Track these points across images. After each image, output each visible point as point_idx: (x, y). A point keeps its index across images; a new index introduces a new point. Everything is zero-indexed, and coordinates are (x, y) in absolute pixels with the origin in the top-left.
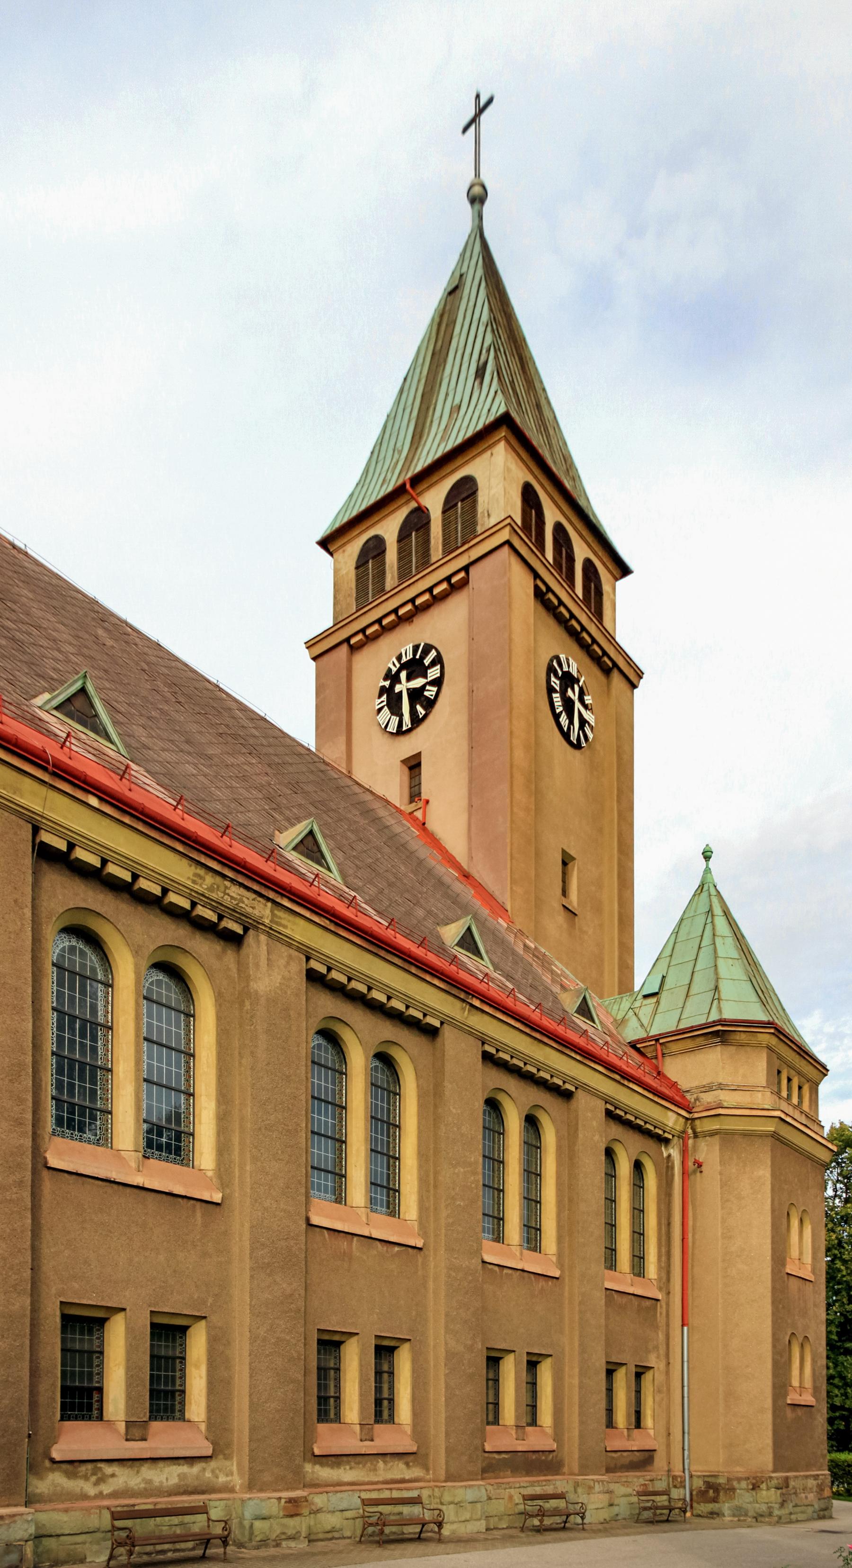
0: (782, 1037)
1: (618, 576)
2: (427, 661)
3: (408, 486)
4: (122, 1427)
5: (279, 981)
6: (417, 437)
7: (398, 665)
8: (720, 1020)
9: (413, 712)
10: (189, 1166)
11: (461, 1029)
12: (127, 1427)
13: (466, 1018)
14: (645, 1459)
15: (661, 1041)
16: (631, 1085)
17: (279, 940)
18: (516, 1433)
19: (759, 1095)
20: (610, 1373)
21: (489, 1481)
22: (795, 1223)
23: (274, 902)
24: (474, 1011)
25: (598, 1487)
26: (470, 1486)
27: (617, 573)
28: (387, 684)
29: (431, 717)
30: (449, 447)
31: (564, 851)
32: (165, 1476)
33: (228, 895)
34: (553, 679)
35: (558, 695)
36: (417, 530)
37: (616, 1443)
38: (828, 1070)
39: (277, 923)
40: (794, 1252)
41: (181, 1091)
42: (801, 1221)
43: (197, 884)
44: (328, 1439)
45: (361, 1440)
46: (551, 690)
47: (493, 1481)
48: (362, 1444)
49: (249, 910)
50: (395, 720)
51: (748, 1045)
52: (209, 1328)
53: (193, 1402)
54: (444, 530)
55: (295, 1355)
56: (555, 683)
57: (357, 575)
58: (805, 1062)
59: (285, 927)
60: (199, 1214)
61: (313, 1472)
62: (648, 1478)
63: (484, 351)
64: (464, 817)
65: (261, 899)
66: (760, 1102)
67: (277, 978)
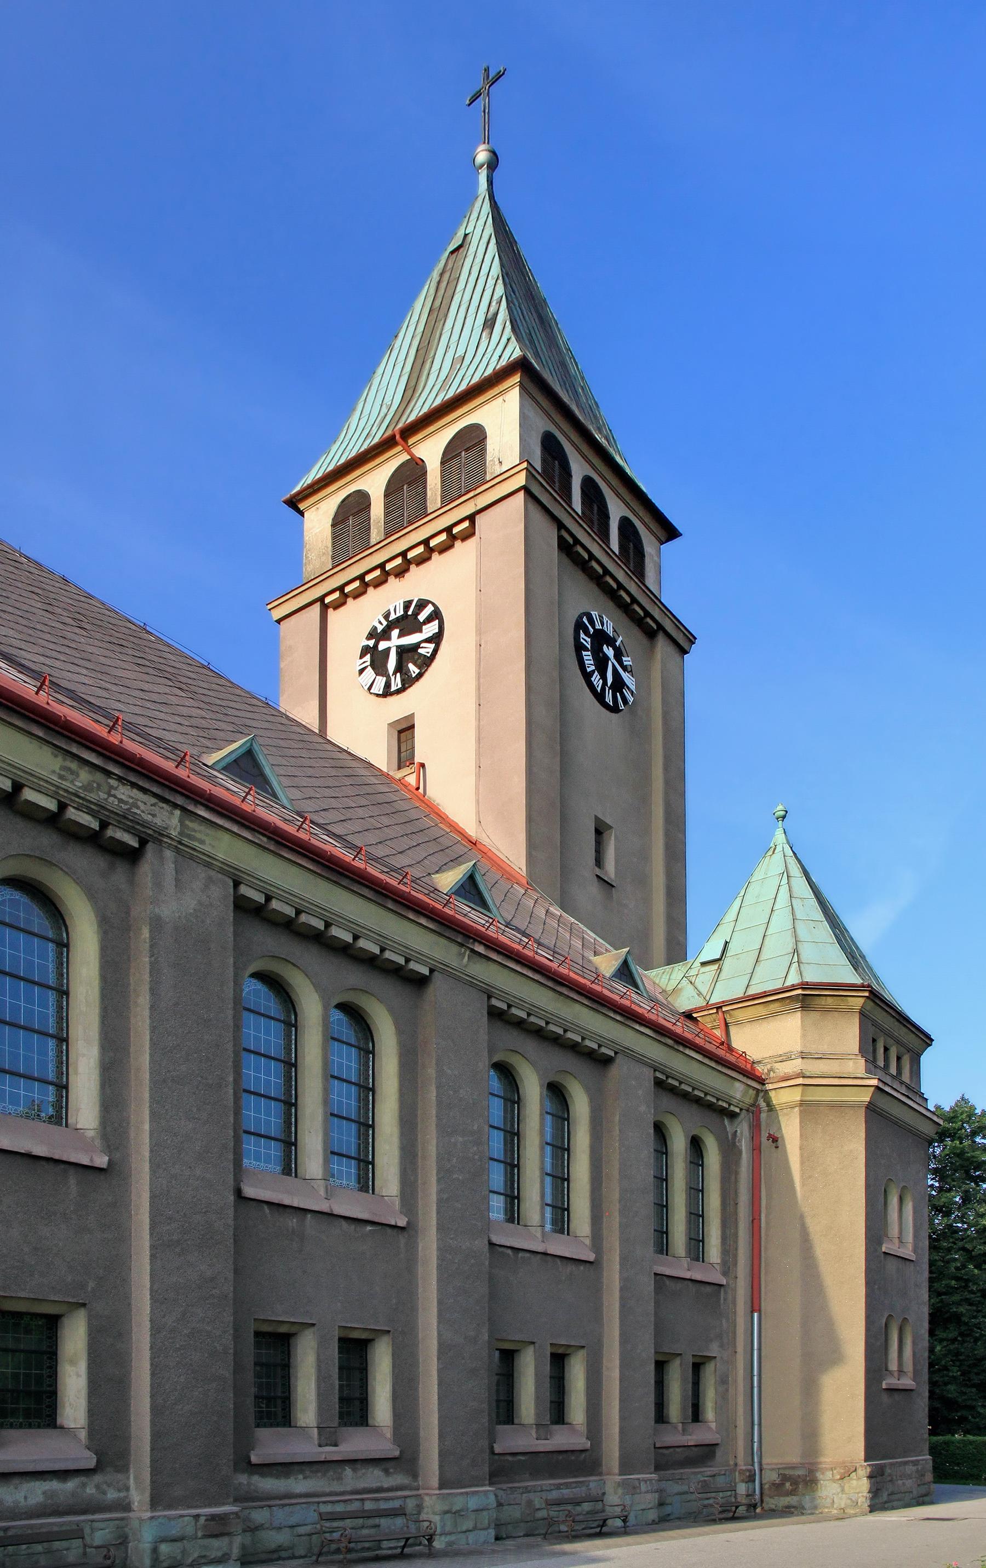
0: (878, 1002)
1: (663, 539)
2: (422, 617)
3: (398, 437)
5: (192, 906)
6: (409, 392)
7: (385, 623)
8: (802, 983)
9: (400, 668)
10: (61, 1125)
11: (458, 979)
13: (466, 966)
14: (707, 1452)
15: (724, 1009)
16: (688, 1052)
17: (192, 858)
18: (537, 1432)
19: (851, 1063)
20: (660, 1366)
21: (499, 1486)
22: (894, 1200)
23: (183, 809)
24: (477, 958)
25: (643, 1487)
27: (662, 534)
28: (371, 643)
29: (427, 675)
30: (450, 394)
31: (597, 818)
32: (23, 1494)
33: (115, 796)
34: (582, 635)
35: (589, 653)
36: (409, 484)
37: (672, 1437)
38: (932, 1040)
39: (189, 836)
40: (894, 1231)
41: (47, 1034)
42: (901, 1200)
43: (66, 780)
44: (271, 1445)
45: (320, 1446)
46: (579, 648)
47: (505, 1486)
48: (321, 1449)
49: (149, 818)
50: (381, 681)
51: (836, 1010)
52: (90, 1319)
53: (67, 1404)
54: (443, 482)
55: (219, 1348)
56: (586, 641)
57: (333, 533)
58: (905, 1030)
59: (202, 842)
61: (249, 1484)
62: (709, 1473)
63: (494, 303)
64: (472, 779)
65: (164, 805)
66: (851, 1071)
67: (190, 902)
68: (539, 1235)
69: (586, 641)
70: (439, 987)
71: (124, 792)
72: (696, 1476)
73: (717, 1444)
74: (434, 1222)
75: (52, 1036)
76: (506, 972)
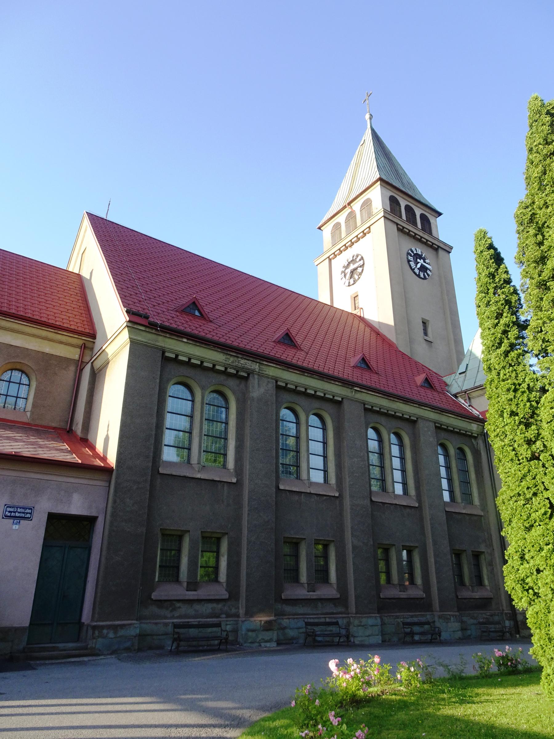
4: (185, 584)
12: (187, 584)
17: (263, 376)
26: (371, 617)
27: (436, 215)
37: (465, 594)
46: (409, 261)
48: (308, 593)
59: (266, 371)
60: (225, 488)
62: (489, 614)
67: (262, 390)
68: (393, 496)
69: (411, 258)
70: (346, 404)
71: (243, 361)
72: (482, 615)
73: (491, 598)
74: (348, 494)
75: (223, 438)
76: (369, 395)
